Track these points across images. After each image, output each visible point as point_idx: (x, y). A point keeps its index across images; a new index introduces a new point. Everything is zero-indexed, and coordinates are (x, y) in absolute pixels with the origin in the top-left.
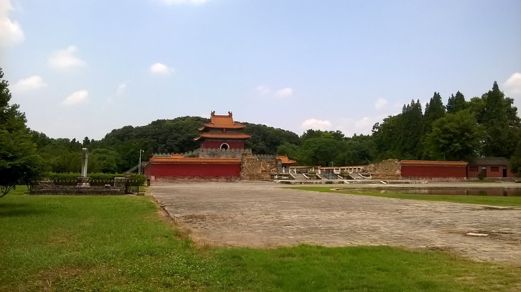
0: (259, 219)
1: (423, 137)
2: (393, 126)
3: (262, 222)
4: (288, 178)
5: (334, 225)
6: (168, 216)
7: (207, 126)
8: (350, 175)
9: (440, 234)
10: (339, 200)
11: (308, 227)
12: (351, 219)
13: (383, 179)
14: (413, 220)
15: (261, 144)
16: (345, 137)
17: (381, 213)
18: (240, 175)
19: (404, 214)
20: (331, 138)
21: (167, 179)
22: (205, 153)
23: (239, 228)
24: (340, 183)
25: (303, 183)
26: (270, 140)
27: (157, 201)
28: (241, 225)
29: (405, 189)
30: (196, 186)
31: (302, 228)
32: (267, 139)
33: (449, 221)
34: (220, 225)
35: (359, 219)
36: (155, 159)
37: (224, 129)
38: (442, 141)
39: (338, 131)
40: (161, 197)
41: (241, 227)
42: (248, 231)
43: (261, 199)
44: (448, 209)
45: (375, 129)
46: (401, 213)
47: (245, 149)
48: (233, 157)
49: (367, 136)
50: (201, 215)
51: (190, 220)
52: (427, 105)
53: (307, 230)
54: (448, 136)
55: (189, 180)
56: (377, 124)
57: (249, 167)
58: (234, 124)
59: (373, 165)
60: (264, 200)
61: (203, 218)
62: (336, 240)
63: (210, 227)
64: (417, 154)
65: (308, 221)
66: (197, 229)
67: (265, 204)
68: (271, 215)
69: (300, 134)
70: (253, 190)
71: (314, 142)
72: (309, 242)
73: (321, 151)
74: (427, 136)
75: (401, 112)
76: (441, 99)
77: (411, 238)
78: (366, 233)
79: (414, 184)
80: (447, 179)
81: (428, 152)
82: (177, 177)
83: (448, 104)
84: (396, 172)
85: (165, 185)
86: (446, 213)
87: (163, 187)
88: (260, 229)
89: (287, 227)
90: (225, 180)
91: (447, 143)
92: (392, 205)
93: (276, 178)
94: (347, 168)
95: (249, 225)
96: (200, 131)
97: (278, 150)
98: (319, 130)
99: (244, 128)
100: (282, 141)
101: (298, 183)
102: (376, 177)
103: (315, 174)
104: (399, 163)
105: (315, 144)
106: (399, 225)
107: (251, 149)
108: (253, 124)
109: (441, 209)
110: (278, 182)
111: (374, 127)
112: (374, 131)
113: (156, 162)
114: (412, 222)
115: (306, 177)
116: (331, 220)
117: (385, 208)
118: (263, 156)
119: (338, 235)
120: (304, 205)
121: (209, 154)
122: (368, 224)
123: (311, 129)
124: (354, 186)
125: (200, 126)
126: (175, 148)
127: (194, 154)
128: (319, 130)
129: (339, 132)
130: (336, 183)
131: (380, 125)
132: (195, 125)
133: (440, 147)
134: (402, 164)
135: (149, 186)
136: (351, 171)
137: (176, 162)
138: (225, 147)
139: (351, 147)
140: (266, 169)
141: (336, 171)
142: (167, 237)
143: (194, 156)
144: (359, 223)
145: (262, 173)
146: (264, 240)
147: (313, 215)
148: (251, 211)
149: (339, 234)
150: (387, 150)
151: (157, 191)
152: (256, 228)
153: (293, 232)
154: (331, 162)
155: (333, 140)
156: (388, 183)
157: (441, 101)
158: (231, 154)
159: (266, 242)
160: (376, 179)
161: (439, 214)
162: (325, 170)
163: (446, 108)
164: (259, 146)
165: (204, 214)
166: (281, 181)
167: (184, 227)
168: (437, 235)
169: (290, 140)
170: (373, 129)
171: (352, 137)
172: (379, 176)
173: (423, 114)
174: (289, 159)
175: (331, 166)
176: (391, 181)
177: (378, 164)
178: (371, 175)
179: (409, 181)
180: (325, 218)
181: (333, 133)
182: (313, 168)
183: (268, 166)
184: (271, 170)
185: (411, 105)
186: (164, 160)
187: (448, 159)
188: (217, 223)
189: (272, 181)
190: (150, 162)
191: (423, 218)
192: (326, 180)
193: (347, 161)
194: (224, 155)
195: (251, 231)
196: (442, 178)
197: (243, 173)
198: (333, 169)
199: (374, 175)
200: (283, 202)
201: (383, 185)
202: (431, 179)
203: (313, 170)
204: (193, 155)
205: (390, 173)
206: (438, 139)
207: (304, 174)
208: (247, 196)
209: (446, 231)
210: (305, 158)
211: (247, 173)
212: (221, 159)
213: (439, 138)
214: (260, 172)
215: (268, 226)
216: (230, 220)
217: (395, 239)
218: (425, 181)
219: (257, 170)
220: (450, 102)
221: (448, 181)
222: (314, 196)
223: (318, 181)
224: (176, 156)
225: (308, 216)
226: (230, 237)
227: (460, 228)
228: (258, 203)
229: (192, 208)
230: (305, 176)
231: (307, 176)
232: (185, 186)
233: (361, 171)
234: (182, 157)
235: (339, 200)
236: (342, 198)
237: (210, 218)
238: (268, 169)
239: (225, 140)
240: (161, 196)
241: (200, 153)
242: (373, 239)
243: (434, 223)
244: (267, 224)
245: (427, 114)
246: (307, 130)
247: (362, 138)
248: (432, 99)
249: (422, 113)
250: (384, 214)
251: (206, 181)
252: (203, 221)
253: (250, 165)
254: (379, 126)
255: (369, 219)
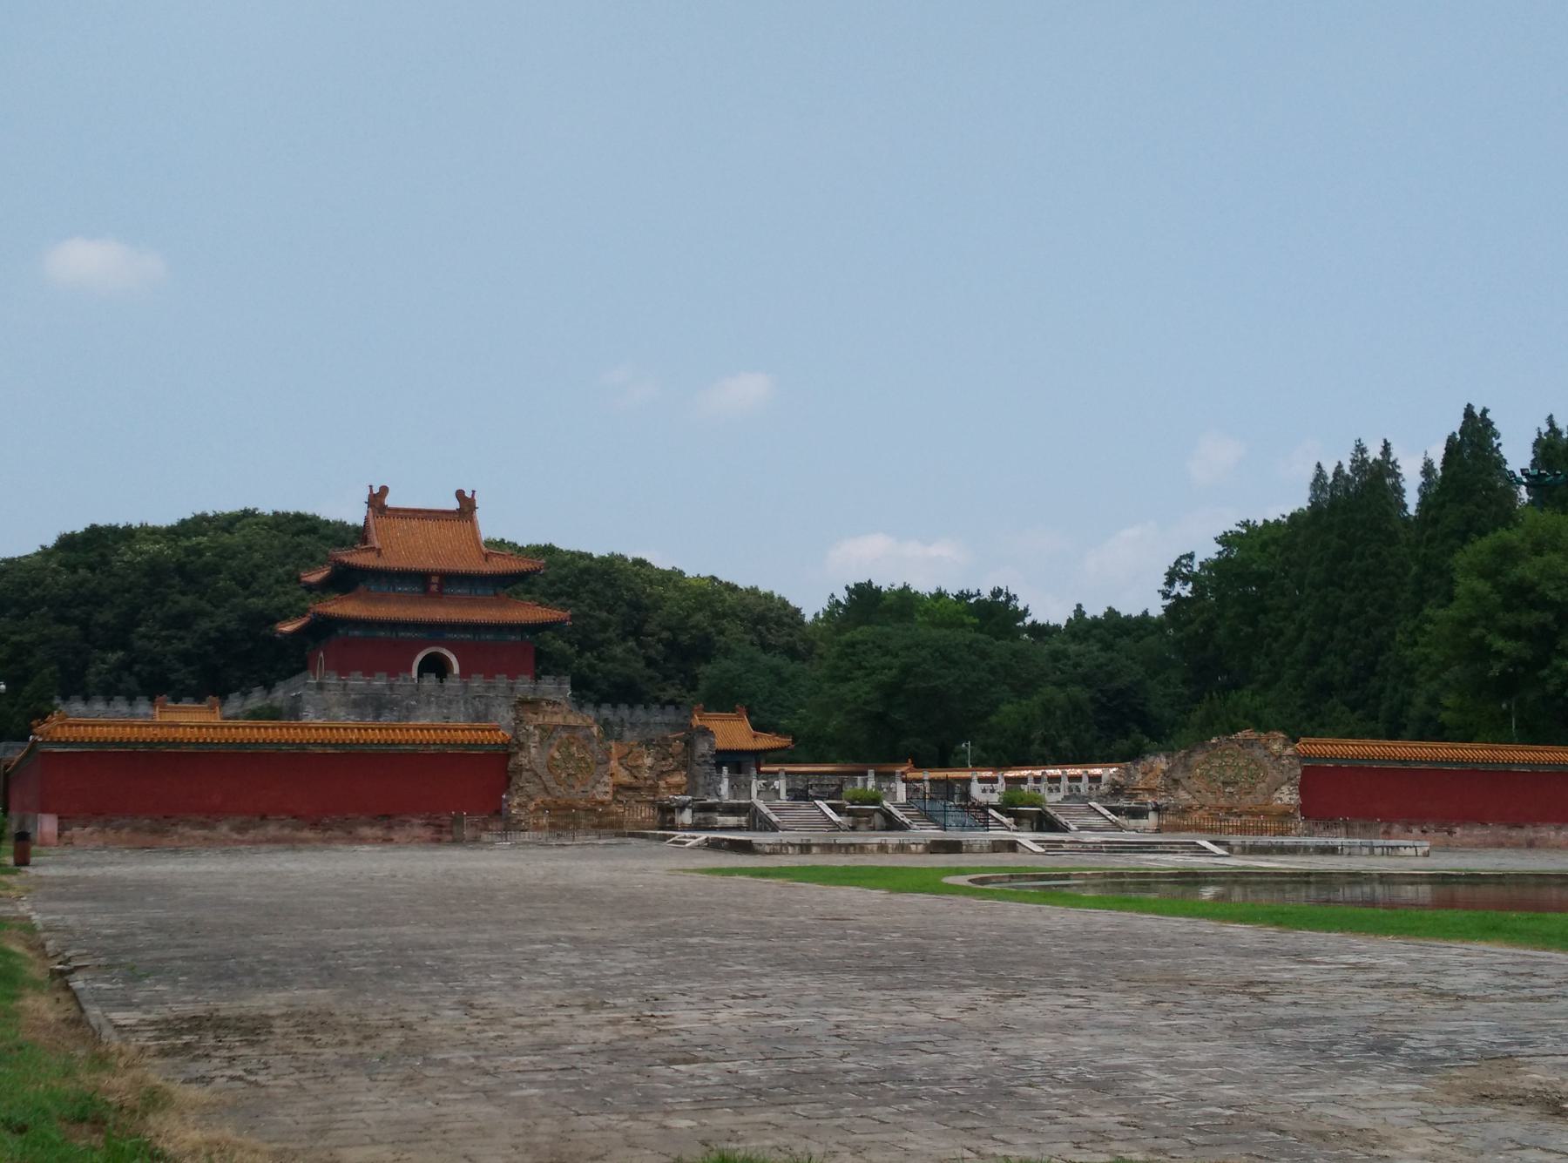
0: (545, 1031)
1: (1411, 625)
2: (1264, 568)
3: (558, 1045)
4: (744, 824)
5: (915, 1060)
6: (78, 1021)
7: (346, 560)
8: (1048, 809)
9: (1430, 1108)
10: (975, 932)
11: (782, 1068)
12: (1005, 1028)
13: (1211, 830)
14: (1311, 1033)
15: (618, 651)
16: (1034, 622)
17: (1166, 995)
18: (505, 806)
19: (1278, 1005)
20: (963, 625)
21: (127, 830)
22: (332, 696)
23: (427, 1077)
24: (997, 847)
25: (814, 850)
26: (665, 634)
27: (43, 946)
28: (445, 1062)
29: (1259, 883)
30: (274, 867)
31: (751, 1072)
32: (649, 628)
33: (1491, 1038)
34: (336, 1063)
35: (1046, 1027)
36: (62, 726)
37: (435, 579)
38: (1500, 644)
39: (1000, 591)
40: (69, 923)
41: (439, 1071)
42: (468, 1095)
43: (584, 930)
44: (1498, 981)
45: (1177, 584)
46: (1263, 1000)
47: (537, 677)
48: (478, 719)
49: (1137, 618)
50: (254, 1013)
51: (187, 1038)
52: (1428, 470)
53: (774, 1083)
54: (1530, 619)
55: (239, 833)
56: (1184, 561)
57: (551, 766)
58: (484, 549)
59: (1164, 760)
60: (598, 934)
61: (254, 1029)
62: (906, 1134)
63: (276, 1078)
64: (1383, 707)
65: (793, 1035)
66: (208, 1089)
67: (599, 952)
68: (615, 1006)
69: (811, 602)
70: (561, 882)
71: (879, 647)
72: (762, 1147)
73: (912, 686)
74: (1431, 621)
75: (1299, 501)
76: (1496, 442)
77: (1284, 1123)
78: (1066, 1096)
79: (1361, 855)
80: (1528, 833)
81: (1434, 701)
82: (173, 821)
83: (1534, 464)
84: (1276, 795)
85: (111, 863)
86: (1485, 999)
87: (95, 872)
88: (532, 1083)
89: (677, 1071)
90: (428, 833)
91: (1528, 654)
92: (1228, 961)
93: (683, 824)
94: (1038, 773)
95: (484, 1063)
96: (310, 588)
97: (703, 686)
98: (906, 588)
99: (536, 571)
100: (722, 638)
101: (793, 845)
102: (1176, 818)
103: (876, 801)
104: (1289, 751)
105: (883, 655)
106: (1237, 1061)
107: (568, 679)
108: (582, 556)
109: (1463, 980)
110: (693, 842)
111: (1172, 577)
112: (1174, 593)
113: (67, 743)
114: (1303, 1046)
115: (835, 817)
116: (906, 1033)
117: (1193, 973)
118: (627, 712)
119: (919, 1110)
120: (794, 955)
121: (356, 704)
122: (1086, 1052)
123: (864, 580)
124: (1063, 862)
125: (311, 560)
126: (177, 671)
127: (277, 704)
128: (906, 588)
129: (1002, 598)
130: (976, 848)
131: (1201, 564)
132: (288, 556)
133: (1491, 674)
134: (1306, 758)
135: (23, 869)
136: (1058, 790)
137: (175, 743)
138: (436, 666)
139: (1058, 673)
140: (636, 777)
141: (984, 791)
142: (22, 1129)
143: (273, 714)
144: (1042, 1047)
145: (614, 798)
146: (538, 1139)
147: (822, 1010)
148: (516, 987)
149: (929, 1103)
150: (1237, 687)
151: (64, 891)
152: (518, 1076)
153: (698, 1095)
154: (963, 745)
155: (974, 635)
156: (1236, 849)
157: (1497, 450)
158: (466, 703)
159: (547, 1147)
160: (1177, 829)
161: (1449, 1005)
162: (927, 784)
163: (1523, 483)
164: (610, 666)
165: (271, 1008)
166: (707, 840)
167: (134, 1080)
168: (1413, 1108)
169: (765, 632)
170: (1165, 584)
171: (1063, 624)
172: (1195, 818)
173: (1412, 510)
174: (759, 727)
175: (962, 765)
176: (1249, 840)
177: (1188, 756)
178: (1154, 810)
179: (1338, 841)
180: (881, 1022)
181: (972, 600)
182: (871, 772)
183: (648, 761)
184: (662, 783)
185: (1351, 470)
186: (108, 732)
187: (1532, 735)
188: (319, 1055)
189: (665, 838)
190: (35, 741)
191: (1363, 1024)
192: (932, 833)
193: (1038, 742)
194: (433, 709)
195: (485, 1092)
196: (1503, 831)
197: (517, 800)
198: (969, 780)
199: (1167, 809)
200: (692, 946)
201: (1210, 860)
202: (1450, 833)
203: (871, 784)
204: (270, 707)
205: (1248, 801)
206: (1484, 636)
207: (822, 804)
208: (521, 916)
209: (1465, 1089)
210: (835, 722)
211: (539, 800)
212: (408, 730)
213: (1484, 631)
214: (603, 792)
215: (580, 1065)
216: (395, 1037)
217: (1198, 1130)
218: (1417, 843)
219: (593, 783)
220: (1544, 455)
221: (1531, 844)
222: (857, 911)
223: (893, 838)
224: (182, 710)
225: (797, 1010)
226: (369, 1125)
227: (1536, 1076)
228: (565, 950)
229: (219, 977)
230: (828, 811)
231: (839, 813)
232: (213, 868)
233: (1104, 788)
234: (216, 719)
235: (975, 932)
236: (990, 924)
237: (291, 1030)
238: (646, 779)
239: (436, 630)
240: (71, 920)
241: (309, 695)
242: (1094, 1132)
243: (1414, 1049)
244: (581, 1054)
245: (1432, 513)
246: (847, 588)
247: (1115, 628)
248: (1451, 439)
249: (1405, 507)
250: (1177, 1003)
251: (328, 841)
252: (251, 1044)
253: (557, 755)
254: (1196, 568)
255: (1098, 1027)
